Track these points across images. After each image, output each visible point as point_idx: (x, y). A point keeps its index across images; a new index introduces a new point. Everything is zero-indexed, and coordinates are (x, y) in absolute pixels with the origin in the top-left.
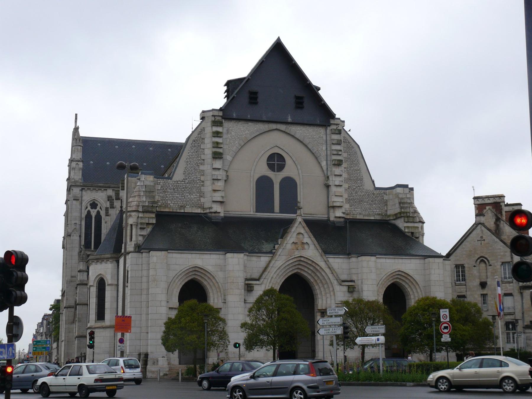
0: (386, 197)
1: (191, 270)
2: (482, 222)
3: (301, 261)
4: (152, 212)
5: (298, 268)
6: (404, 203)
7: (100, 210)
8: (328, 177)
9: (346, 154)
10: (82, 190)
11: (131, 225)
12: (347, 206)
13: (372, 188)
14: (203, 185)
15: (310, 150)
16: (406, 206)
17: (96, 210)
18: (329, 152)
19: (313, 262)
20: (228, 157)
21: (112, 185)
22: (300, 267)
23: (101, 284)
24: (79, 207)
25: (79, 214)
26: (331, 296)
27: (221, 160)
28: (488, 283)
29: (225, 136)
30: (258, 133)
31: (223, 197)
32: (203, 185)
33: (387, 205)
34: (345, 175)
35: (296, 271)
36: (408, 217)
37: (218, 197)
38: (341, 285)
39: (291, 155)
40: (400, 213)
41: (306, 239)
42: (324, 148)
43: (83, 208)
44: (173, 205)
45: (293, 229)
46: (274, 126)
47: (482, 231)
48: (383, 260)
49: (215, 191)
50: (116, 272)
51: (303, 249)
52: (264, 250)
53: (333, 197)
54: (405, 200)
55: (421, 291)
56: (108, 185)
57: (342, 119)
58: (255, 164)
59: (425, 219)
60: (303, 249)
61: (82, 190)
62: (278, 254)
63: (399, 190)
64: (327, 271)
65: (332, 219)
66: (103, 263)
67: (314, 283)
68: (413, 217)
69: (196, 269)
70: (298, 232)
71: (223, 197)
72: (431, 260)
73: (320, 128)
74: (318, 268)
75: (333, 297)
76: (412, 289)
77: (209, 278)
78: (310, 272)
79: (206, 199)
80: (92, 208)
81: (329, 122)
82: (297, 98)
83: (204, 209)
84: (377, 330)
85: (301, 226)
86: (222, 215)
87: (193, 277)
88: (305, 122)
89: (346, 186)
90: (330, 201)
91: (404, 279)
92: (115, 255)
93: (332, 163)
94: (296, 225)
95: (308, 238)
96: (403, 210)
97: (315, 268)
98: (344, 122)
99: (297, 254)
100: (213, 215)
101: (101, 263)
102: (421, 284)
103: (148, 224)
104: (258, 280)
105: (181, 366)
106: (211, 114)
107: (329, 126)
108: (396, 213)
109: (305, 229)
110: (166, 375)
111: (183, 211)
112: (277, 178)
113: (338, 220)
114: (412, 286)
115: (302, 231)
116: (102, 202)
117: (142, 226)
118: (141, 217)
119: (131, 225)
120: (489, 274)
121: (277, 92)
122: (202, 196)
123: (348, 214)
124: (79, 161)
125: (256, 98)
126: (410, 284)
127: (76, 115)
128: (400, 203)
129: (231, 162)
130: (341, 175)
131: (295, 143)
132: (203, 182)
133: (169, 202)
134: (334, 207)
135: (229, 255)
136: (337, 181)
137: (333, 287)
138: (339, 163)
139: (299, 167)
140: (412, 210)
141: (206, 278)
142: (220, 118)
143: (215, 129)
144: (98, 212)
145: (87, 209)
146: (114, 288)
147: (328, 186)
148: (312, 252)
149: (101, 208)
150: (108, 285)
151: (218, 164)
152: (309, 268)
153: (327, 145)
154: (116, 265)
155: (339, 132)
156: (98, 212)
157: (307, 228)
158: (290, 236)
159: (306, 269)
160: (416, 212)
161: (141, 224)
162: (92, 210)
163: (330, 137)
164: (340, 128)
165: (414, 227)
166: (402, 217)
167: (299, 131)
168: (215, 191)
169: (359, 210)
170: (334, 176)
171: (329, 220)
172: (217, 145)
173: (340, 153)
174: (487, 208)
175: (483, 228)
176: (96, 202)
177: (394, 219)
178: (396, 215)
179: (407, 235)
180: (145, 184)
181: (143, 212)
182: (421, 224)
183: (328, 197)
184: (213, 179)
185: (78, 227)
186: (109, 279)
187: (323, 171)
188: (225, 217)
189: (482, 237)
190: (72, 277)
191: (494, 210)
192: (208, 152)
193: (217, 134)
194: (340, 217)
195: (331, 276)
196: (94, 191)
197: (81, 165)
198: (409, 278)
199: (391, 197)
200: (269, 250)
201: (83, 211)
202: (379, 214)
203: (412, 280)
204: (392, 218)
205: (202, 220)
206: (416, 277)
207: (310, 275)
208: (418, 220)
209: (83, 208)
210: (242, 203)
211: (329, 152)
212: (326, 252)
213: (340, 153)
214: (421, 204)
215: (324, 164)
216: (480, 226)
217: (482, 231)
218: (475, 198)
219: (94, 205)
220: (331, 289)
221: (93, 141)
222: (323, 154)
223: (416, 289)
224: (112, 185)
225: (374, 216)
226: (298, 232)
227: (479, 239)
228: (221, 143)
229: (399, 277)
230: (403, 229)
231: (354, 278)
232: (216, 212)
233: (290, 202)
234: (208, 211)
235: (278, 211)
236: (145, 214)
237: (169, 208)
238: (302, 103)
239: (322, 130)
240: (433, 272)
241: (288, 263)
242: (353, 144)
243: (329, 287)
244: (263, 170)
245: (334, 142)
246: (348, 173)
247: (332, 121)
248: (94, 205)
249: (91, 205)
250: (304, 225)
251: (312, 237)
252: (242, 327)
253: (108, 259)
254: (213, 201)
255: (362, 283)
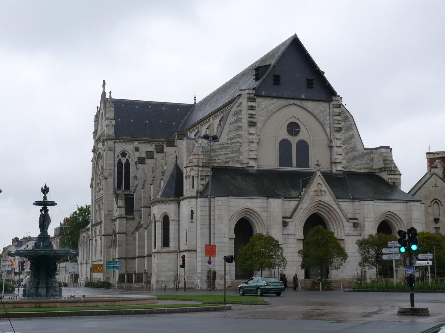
0: (372, 156)
1: (244, 211)
2: (436, 172)
3: (321, 204)
4: (208, 167)
5: (318, 209)
6: (387, 160)
7: (128, 158)
8: (331, 141)
9: (344, 124)
10: (114, 143)
11: (193, 177)
12: (344, 162)
13: (362, 149)
14: (241, 146)
15: (318, 119)
16: (388, 162)
17: (125, 159)
18: (331, 122)
19: (328, 204)
20: (259, 125)
21: (138, 139)
22: (319, 208)
23: (166, 220)
24: (113, 156)
25: (110, 162)
26: (341, 230)
27: (255, 128)
28: (440, 219)
29: (257, 109)
30: (280, 107)
31: (257, 155)
32: (241, 146)
33: (373, 161)
34: (343, 139)
35: (315, 211)
36: (391, 171)
37: (253, 155)
38: (348, 222)
39: (304, 123)
40: (385, 168)
41: (324, 188)
42: (328, 118)
43: (116, 156)
44: (220, 162)
45: (315, 181)
46: (292, 102)
47: (436, 179)
48: (377, 204)
49: (251, 150)
50: (178, 212)
51: (322, 195)
52: (293, 196)
53: (335, 155)
54: (388, 158)
55: (404, 226)
56: (134, 139)
57: (341, 96)
58: (279, 129)
59: (401, 172)
60: (322, 195)
61: (114, 143)
62: (304, 199)
63: (383, 150)
64: (339, 211)
65: (334, 171)
66: (167, 204)
67: (329, 220)
68: (394, 171)
69: (248, 210)
70: (318, 183)
71: (257, 155)
72: (412, 203)
73: (325, 103)
74: (332, 209)
75: (343, 231)
76: (397, 225)
77: (256, 216)
78: (326, 212)
79: (243, 156)
80: (122, 157)
81: (332, 98)
82: (308, 80)
83: (242, 164)
84: (427, 256)
85: (320, 178)
86: (256, 168)
87: (244, 215)
88: (315, 99)
89: (344, 147)
90: (332, 158)
91: (392, 217)
92: (176, 198)
93: (334, 130)
94: (317, 177)
95: (325, 187)
96: (386, 166)
97: (330, 209)
98: (341, 98)
99: (318, 199)
100: (250, 168)
101: (165, 204)
102: (405, 221)
103: (207, 176)
104: (290, 218)
105: (237, 280)
106: (247, 92)
107: (332, 101)
108: (380, 167)
109: (323, 181)
110: (230, 287)
111: (227, 166)
112: (294, 140)
113: (339, 172)
114: (398, 223)
115: (321, 182)
116: (130, 152)
117: (203, 178)
118: (201, 171)
119: (193, 177)
120: (441, 212)
121: (291, 73)
122: (240, 154)
123: (345, 168)
124: (112, 119)
125: (279, 80)
126: (396, 221)
127: (104, 81)
128: (384, 160)
129: (261, 129)
130: (341, 139)
131: (307, 115)
132: (241, 143)
133: (217, 159)
134: (335, 163)
135: (271, 200)
136: (338, 143)
137: (342, 223)
138: (339, 130)
139: (310, 132)
140: (393, 166)
141: (254, 217)
142: (253, 95)
143: (250, 104)
144: (127, 160)
145: (119, 158)
146: (176, 223)
147: (331, 147)
148: (328, 197)
149: (129, 157)
150: (172, 220)
151: (253, 130)
152: (325, 209)
153: (330, 116)
154: (177, 205)
155: (340, 106)
156: (127, 160)
157: (324, 180)
158: (312, 185)
159: (323, 210)
160: (395, 167)
161: (202, 176)
162: (122, 159)
163: (333, 110)
164: (339, 103)
165: (395, 178)
166: (385, 171)
167: (309, 105)
168: (251, 150)
169: (352, 165)
170: (335, 140)
171: (332, 172)
172: (252, 116)
173: (340, 122)
174: (437, 161)
175: (437, 177)
176: (126, 152)
177: (379, 172)
178: (380, 169)
179: (390, 185)
180: (202, 145)
181: (202, 167)
182: (399, 176)
183: (331, 155)
184: (250, 142)
185: (112, 172)
186: (172, 216)
187: (327, 136)
188: (258, 170)
189: (435, 184)
190: (109, 211)
191: (442, 163)
192: (245, 121)
193: (252, 108)
194: (340, 171)
195: (341, 215)
196: (124, 143)
197: (114, 122)
198: (396, 216)
199: (376, 155)
200: (296, 196)
201: (116, 159)
202: (367, 168)
203: (398, 218)
204: (377, 171)
205: (242, 172)
206: (401, 216)
207: (326, 214)
208: (398, 173)
209: (116, 156)
210: (270, 160)
211: (331, 121)
212: (338, 197)
213: (340, 122)
214: (398, 159)
215: (328, 130)
216: (434, 176)
217: (436, 179)
218: (427, 154)
219: (124, 154)
220: (341, 225)
221: (118, 102)
222: (328, 122)
223: (401, 225)
224: (138, 139)
225: (364, 169)
226: (318, 183)
227: (434, 185)
228: (255, 115)
229: (389, 216)
230: (387, 180)
231: (358, 216)
232: (252, 167)
233: (304, 159)
234: (245, 166)
235: (295, 166)
236: (204, 168)
237: (218, 163)
238: (312, 84)
239: (326, 105)
240: (413, 212)
241: (311, 206)
242: (349, 115)
243: (339, 223)
244: (285, 135)
245: (335, 114)
246: (345, 137)
247: (334, 98)
248: (124, 154)
249: (121, 154)
250: (322, 177)
251: (328, 186)
252: (299, 253)
253: (171, 201)
254: (250, 158)
255: (364, 220)
